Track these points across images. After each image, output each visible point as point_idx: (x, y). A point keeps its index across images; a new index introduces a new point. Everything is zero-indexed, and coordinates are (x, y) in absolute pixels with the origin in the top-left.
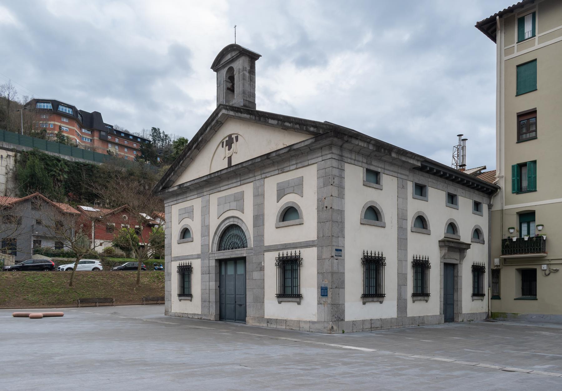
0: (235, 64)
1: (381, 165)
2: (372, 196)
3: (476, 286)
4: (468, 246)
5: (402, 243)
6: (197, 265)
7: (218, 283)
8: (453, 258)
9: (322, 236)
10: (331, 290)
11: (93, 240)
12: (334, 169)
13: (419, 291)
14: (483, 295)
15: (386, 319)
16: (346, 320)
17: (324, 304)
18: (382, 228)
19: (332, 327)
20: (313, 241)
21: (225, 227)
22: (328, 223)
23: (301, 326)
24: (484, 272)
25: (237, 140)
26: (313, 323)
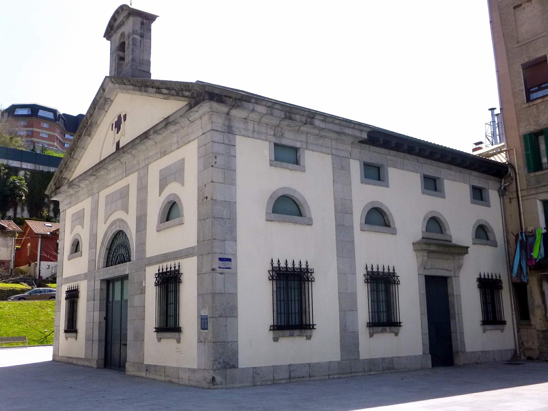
0: (129, 33)
1: (303, 138)
2: (284, 179)
3: (171, 307)
4: (464, 250)
5: (345, 246)
6: (84, 289)
7: (104, 313)
8: (440, 267)
9: (202, 240)
10: (212, 320)
11: (38, 262)
12: (216, 144)
13: (491, 318)
14: (504, 323)
15: (318, 364)
16: (240, 366)
17: (204, 343)
18: (309, 226)
19: (213, 379)
20: (193, 248)
21: (111, 234)
22: (208, 221)
23: (180, 377)
24: (501, 288)
25: (125, 120)
26: (193, 371)
